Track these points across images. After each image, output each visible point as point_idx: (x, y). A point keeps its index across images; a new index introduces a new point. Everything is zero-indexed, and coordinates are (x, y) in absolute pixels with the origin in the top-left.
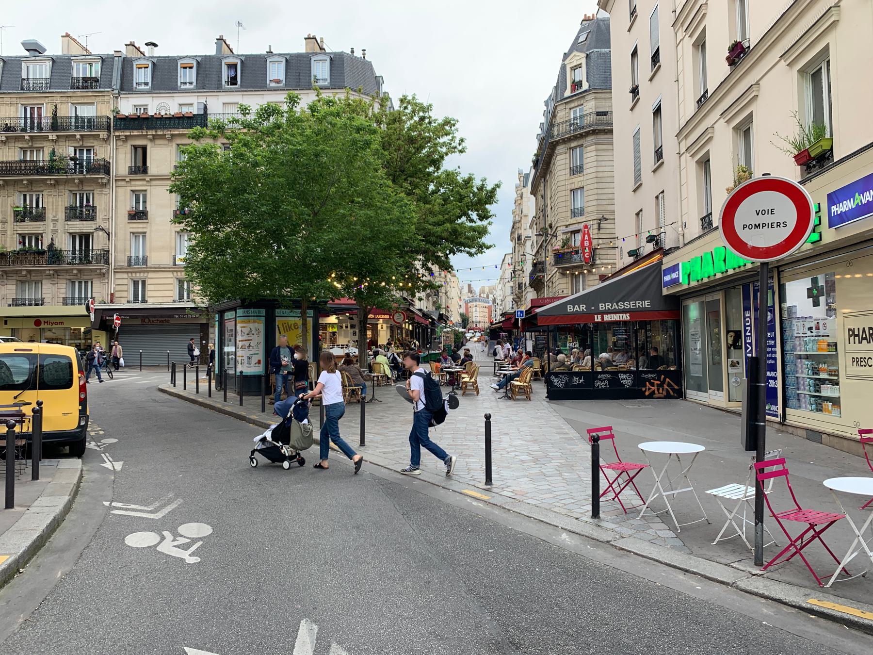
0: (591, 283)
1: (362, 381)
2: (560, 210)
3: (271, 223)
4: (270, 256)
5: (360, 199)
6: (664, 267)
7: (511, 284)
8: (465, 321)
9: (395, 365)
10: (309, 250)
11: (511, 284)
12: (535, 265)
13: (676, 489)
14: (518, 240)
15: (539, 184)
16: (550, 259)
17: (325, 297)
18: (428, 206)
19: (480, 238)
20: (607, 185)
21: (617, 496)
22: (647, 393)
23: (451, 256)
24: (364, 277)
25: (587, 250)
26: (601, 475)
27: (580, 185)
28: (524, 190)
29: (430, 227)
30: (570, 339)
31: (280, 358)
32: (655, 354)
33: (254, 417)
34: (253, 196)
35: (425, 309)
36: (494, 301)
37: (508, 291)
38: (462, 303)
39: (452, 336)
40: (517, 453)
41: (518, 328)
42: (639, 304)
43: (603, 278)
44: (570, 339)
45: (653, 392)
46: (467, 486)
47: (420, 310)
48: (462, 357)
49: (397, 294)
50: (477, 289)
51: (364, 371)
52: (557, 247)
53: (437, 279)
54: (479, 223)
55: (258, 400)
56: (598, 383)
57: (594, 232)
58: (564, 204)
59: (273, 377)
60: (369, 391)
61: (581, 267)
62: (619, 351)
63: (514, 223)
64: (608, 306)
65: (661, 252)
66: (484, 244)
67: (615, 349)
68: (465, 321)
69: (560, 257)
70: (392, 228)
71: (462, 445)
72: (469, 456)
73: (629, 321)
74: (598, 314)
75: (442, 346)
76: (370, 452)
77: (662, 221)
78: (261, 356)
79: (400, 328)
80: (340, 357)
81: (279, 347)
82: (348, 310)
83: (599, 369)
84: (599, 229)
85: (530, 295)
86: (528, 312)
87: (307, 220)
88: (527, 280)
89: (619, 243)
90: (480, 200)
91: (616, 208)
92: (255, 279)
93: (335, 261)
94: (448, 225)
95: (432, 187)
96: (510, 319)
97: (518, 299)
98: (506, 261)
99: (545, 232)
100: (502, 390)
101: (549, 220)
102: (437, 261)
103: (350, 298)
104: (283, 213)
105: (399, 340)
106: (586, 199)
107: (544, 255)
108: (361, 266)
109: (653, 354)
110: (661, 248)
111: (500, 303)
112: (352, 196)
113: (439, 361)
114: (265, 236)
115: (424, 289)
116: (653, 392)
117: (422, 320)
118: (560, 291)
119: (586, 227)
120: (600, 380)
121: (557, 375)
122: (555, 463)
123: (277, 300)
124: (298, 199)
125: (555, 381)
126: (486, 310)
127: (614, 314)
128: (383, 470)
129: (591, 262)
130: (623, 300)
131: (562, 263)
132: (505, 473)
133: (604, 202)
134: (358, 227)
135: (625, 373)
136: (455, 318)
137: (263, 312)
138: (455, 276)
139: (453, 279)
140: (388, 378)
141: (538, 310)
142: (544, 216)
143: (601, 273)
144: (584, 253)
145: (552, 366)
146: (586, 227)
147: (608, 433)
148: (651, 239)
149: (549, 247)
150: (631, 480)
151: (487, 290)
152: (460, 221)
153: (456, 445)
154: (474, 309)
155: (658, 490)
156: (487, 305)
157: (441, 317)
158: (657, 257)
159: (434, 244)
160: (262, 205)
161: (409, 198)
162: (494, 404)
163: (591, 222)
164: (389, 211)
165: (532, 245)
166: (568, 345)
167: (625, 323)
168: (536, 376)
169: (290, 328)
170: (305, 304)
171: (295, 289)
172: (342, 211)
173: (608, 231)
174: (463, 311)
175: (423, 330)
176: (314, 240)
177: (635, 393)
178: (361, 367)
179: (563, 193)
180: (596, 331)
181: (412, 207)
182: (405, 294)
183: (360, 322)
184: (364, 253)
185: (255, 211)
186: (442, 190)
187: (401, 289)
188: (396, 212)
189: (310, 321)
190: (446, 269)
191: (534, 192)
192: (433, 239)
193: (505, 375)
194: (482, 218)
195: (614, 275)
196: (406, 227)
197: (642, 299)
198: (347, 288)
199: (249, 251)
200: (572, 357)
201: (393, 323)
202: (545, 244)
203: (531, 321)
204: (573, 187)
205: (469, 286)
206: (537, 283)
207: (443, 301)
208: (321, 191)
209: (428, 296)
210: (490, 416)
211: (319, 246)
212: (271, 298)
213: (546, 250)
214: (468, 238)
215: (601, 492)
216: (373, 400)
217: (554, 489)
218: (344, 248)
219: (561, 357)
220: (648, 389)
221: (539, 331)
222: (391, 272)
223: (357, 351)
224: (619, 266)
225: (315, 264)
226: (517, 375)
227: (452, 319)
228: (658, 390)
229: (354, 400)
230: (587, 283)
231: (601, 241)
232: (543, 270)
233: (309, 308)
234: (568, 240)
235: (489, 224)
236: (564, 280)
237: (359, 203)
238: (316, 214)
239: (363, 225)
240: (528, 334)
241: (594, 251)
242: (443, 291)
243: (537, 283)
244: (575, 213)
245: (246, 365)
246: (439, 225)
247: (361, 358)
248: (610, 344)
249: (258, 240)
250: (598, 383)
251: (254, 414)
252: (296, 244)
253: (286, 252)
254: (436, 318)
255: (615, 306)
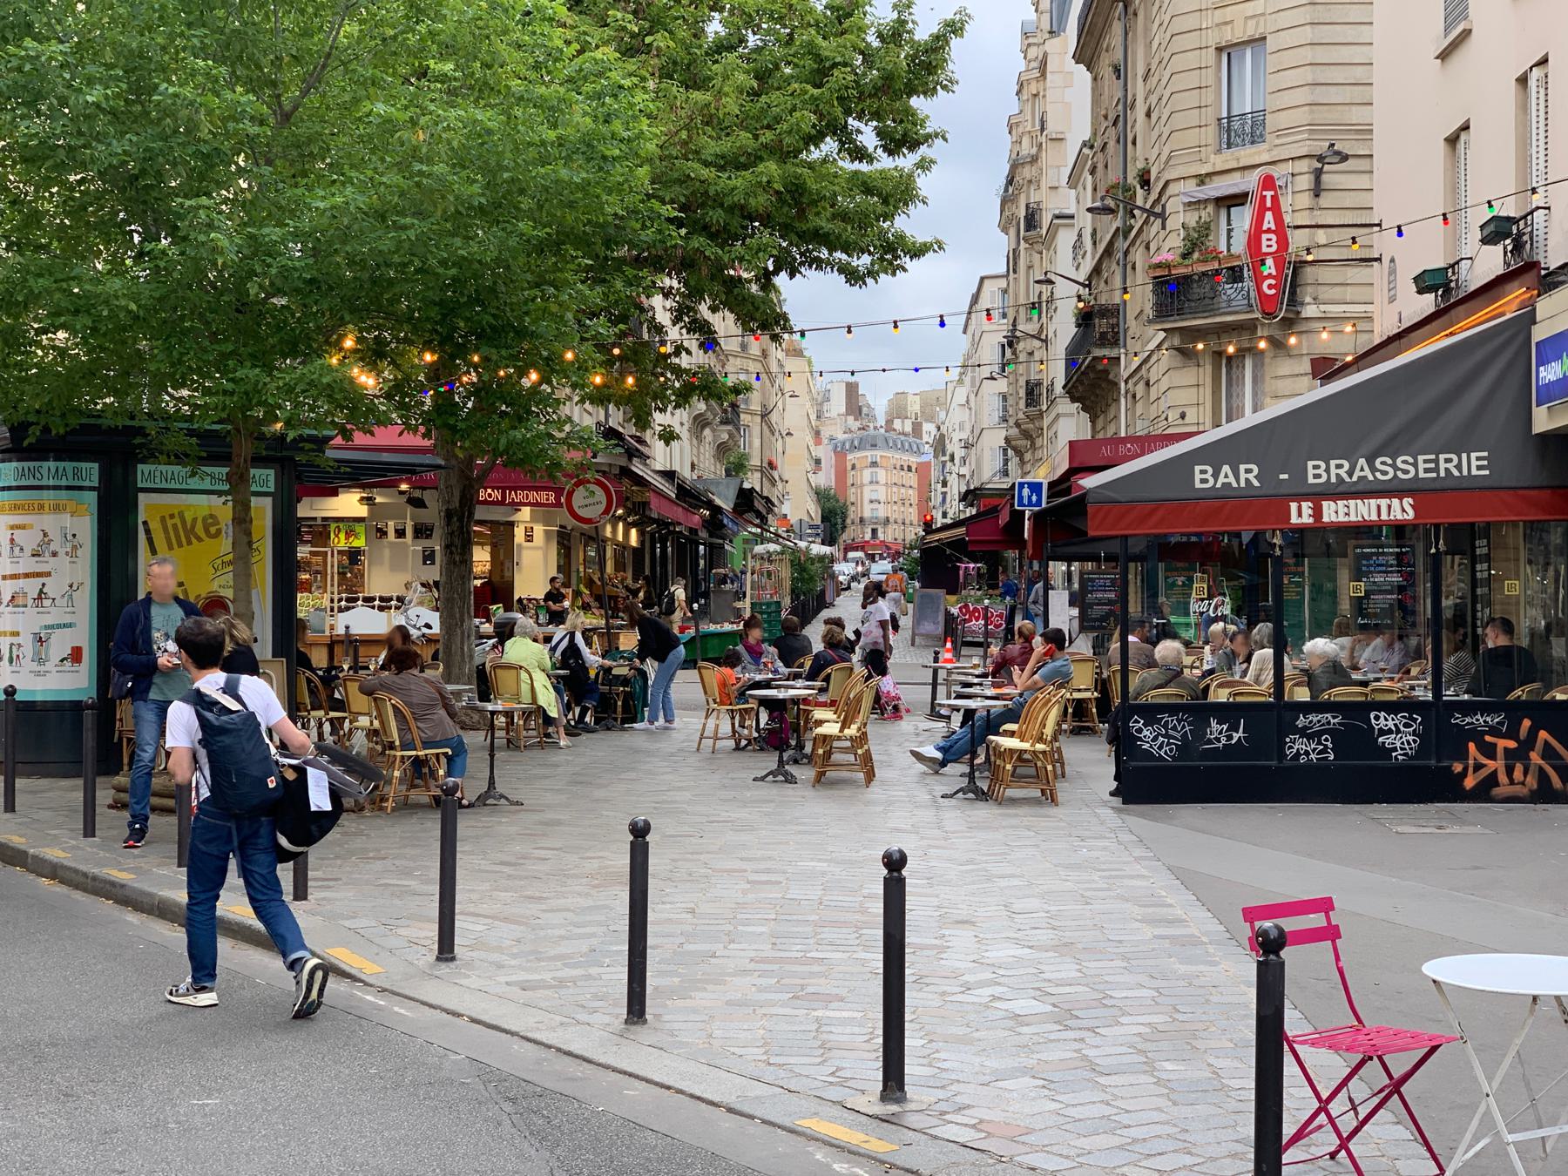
0: (1284, 386)
1: (452, 730)
2: (1179, 121)
3: (120, 147)
4: (116, 267)
5: (448, 67)
6: (1539, 333)
7: (1002, 385)
8: (833, 520)
9: (572, 677)
10: (258, 249)
11: (1002, 385)
12: (1085, 319)
13: (1554, 1122)
14: (1028, 227)
15: (1107, 24)
16: (1140, 298)
17: (318, 423)
18: (697, 96)
19: (888, 216)
20: (1350, 34)
21: (1344, 1144)
22: (1469, 783)
23: (781, 280)
24: (462, 351)
25: (1269, 267)
26: (1290, 1068)
27: (1251, 31)
28: (1053, 46)
29: (705, 173)
30: (1200, 586)
31: (148, 641)
32: (1503, 641)
33: (54, 854)
34: (55, 47)
35: (686, 473)
36: (940, 445)
37: (990, 409)
38: (824, 452)
39: (785, 572)
40: (997, 991)
41: (1020, 544)
42: (1448, 464)
43: (1325, 368)
44: (1200, 586)
45: (1492, 780)
46: (814, 1105)
47: (669, 475)
48: (818, 646)
49: (585, 417)
50: (878, 401)
51: (458, 694)
52: (1164, 256)
53: (733, 365)
54: (885, 162)
55: (69, 792)
56: (1298, 745)
57: (1296, 204)
58: (1192, 99)
59: (124, 710)
60: (476, 764)
61: (1249, 327)
62: (1377, 630)
63: (1015, 166)
64: (1338, 469)
65: (1530, 277)
66: (901, 237)
67: (1363, 622)
68: (833, 520)
69: (1173, 292)
70: (564, 173)
71: (805, 961)
72: (827, 1000)
73: (1415, 527)
74: (1300, 497)
75: (746, 606)
76: (473, 982)
77: (1538, 164)
78: (83, 634)
79: (595, 538)
80: (372, 641)
81: (148, 600)
82: (407, 470)
83: (1303, 695)
84: (1317, 191)
85: (1069, 425)
86: (1060, 486)
87: (251, 139)
88: (1056, 373)
89: (1384, 243)
90: (888, 78)
91: (1378, 117)
92: (62, 352)
93: (356, 293)
94: (770, 168)
95: (715, 27)
96: (994, 511)
97: (1024, 440)
98: (985, 302)
99: (1125, 200)
100: (957, 769)
101: (1142, 154)
102: (732, 297)
103: (408, 427)
104: (166, 112)
105: (590, 583)
106: (1275, 82)
107: (1117, 282)
108: (449, 310)
109: (1494, 640)
110: (1532, 266)
111: (959, 453)
112: (420, 52)
113: (732, 660)
114: (99, 197)
115: (683, 398)
116: (1492, 780)
117: (676, 513)
118: (1173, 415)
119: (1268, 183)
120: (1303, 732)
121: (1151, 713)
122: (1131, 1027)
123: (141, 431)
124: (220, 60)
125: (1147, 736)
126: (912, 479)
127: (1359, 497)
128: (517, 1046)
129: (1286, 306)
130: (1391, 447)
131: (1181, 313)
132: (953, 1059)
133: (1334, 95)
134: (440, 168)
135: (1391, 708)
136: (797, 506)
137: (91, 471)
138: (798, 353)
139: (791, 364)
140: (548, 721)
141: (1090, 482)
142: (1122, 140)
143: (1320, 351)
144: (1259, 279)
145: (1135, 682)
146: (1268, 183)
147: (1316, 920)
148: (1497, 230)
149: (1138, 256)
150: (1396, 1086)
151: (914, 406)
152: (815, 154)
153: (782, 960)
154: (867, 475)
155: (1487, 1124)
156: (913, 460)
157: (746, 500)
158: (1516, 295)
159: (722, 236)
160: (90, 81)
161: (631, 65)
162: (928, 815)
163: (1289, 167)
164: (553, 113)
165: (1077, 246)
166: (1194, 607)
167: (1400, 530)
168: (1078, 718)
169: (190, 532)
170: (245, 448)
171: (207, 392)
172: (380, 108)
173: (1349, 200)
174: (825, 479)
175: (680, 550)
176: (280, 214)
177: (1427, 782)
178: (448, 677)
179: (1192, 59)
180: (1299, 557)
181: (639, 97)
182: (616, 417)
183: (449, 515)
184: (461, 263)
185: (63, 102)
186: (753, 40)
187: (600, 398)
188: (580, 117)
189: (263, 511)
190: (764, 326)
191: (1086, 54)
192: (716, 216)
193: (969, 714)
194: (896, 143)
195: (1365, 358)
196: (618, 172)
197: (1459, 445)
198: (397, 391)
199: (39, 248)
200: (1205, 650)
201: (571, 523)
202: (1121, 245)
203: (1065, 522)
204: (1228, 36)
205: (852, 389)
206: (1092, 385)
207: (753, 445)
208: (306, 33)
209: (700, 423)
210: (902, 860)
211: (296, 236)
212: (121, 422)
213: (1127, 267)
214: (844, 217)
215: (1288, 1130)
216: (489, 797)
217: (1125, 1119)
218: (386, 245)
219: (1167, 649)
220: (1473, 766)
221: (1095, 558)
222: (560, 336)
223: (434, 619)
224: (1385, 326)
225: (280, 301)
226: (1012, 715)
227: (785, 509)
228: (1510, 771)
229: (420, 796)
230: (1270, 385)
231: (1321, 236)
232: (1113, 338)
233: (259, 461)
234: (1205, 229)
235: (925, 165)
236: (1188, 376)
237: (443, 78)
238: (286, 117)
239: (460, 162)
240: (1057, 569)
241: (1294, 274)
242: (755, 406)
243: (1092, 385)
244: (1233, 131)
245: (28, 664)
246: (745, 167)
247: (447, 648)
248: (1345, 606)
249: (76, 210)
250: (1298, 745)
251: (54, 841)
252: (210, 226)
253: (173, 252)
254: (725, 502)
255: (1363, 470)
